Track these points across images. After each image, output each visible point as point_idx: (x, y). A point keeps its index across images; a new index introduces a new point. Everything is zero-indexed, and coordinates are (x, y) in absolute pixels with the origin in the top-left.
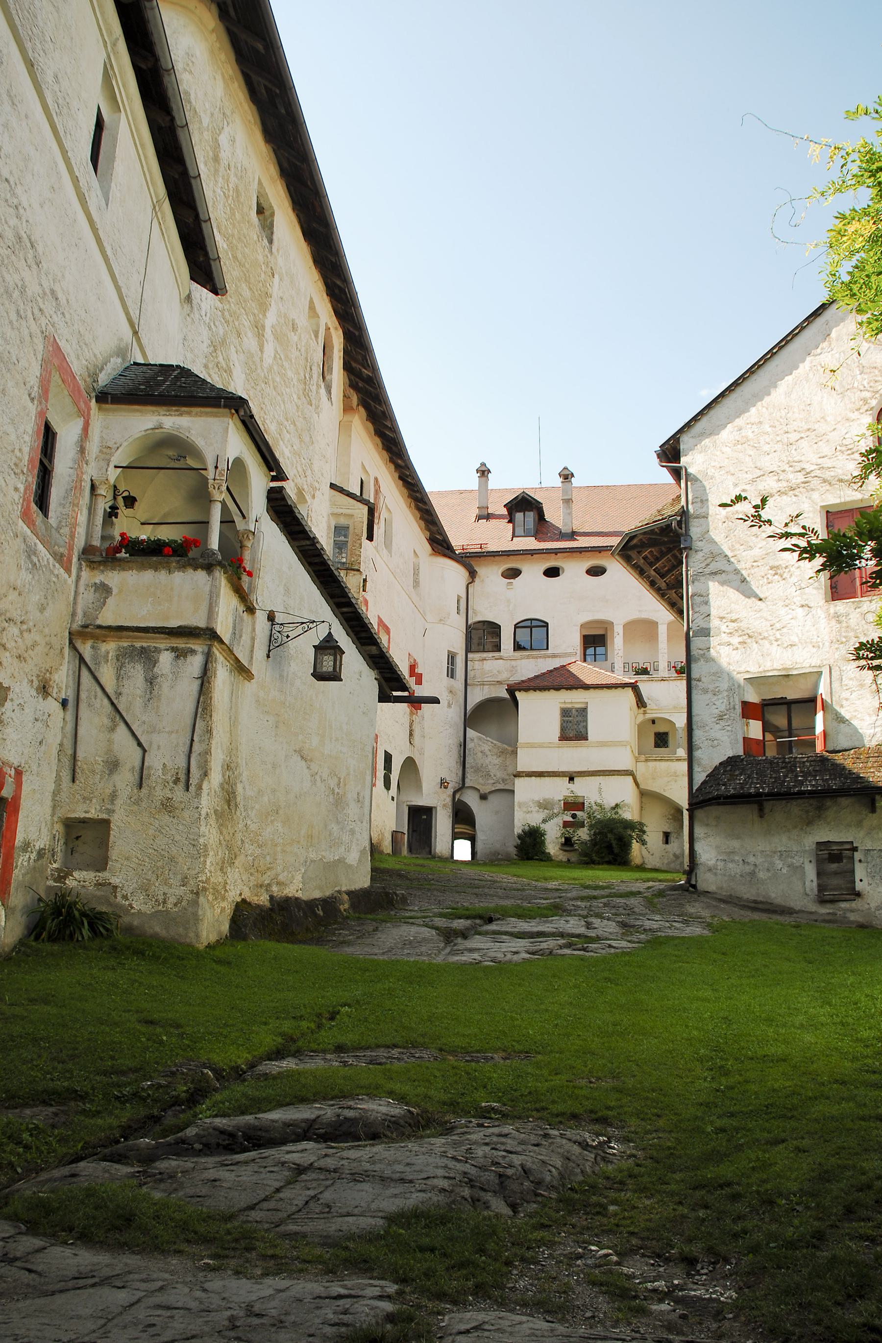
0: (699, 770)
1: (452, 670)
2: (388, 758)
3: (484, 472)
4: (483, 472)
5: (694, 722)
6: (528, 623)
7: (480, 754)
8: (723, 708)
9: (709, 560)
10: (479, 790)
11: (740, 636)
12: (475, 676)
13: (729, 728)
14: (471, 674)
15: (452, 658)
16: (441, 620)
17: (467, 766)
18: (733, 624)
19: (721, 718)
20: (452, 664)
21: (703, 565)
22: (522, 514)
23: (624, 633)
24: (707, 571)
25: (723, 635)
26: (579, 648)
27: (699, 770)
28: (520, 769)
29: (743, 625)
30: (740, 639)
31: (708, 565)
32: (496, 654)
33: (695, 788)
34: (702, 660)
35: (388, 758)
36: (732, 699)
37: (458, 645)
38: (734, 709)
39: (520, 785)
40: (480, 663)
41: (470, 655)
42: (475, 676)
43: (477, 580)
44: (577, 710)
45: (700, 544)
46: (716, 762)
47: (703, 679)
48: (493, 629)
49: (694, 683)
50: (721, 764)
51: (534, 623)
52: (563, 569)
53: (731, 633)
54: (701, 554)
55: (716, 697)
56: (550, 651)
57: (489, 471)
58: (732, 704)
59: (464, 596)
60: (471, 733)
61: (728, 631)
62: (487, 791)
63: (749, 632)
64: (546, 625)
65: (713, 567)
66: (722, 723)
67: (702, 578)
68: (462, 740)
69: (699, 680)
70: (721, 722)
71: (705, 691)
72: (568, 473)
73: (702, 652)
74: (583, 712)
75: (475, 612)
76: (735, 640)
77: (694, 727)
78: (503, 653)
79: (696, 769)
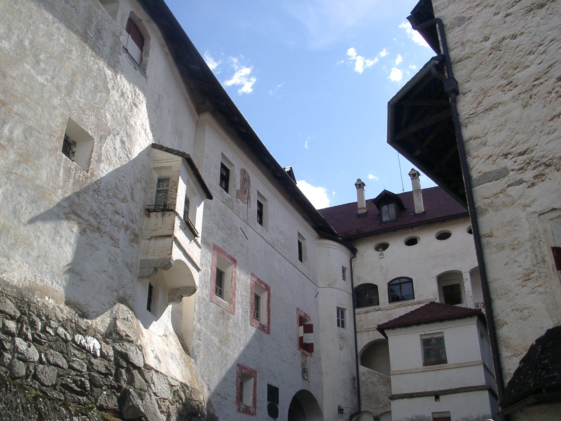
0: (509, 354)
1: (343, 322)
2: (273, 392)
3: (360, 185)
4: (360, 185)
5: (491, 290)
6: (398, 281)
7: (370, 385)
8: (528, 264)
9: (480, 99)
10: (372, 413)
11: (534, 168)
12: (362, 326)
13: (541, 289)
14: (358, 324)
15: (341, 312)
16: (329, 285)
17: (362, 394)
18: (521, 157)
19: (527, 278)
20: (343, 317)
21: (475, 105)
22: (386, 206)
23: (471, 279)
24: (480, 109)
25: (511, 173)
26: (437, 294)
27: (509, 354)
28: (394, 392)
29: (536, 154)
30: (536, 172)
31: (480, 103)
32: (376, 307)
33: (507, 380)
34: (490, 210)
35: (273, 392)
36: (538, 250)
37: (347, 302)
38: (544, 261)
39: (396, 405)
40: (365, 315)
41: (357, 310)
42: (362, 326)
43: (358, 255)
44: (436, 339)
45: (467, 85)
46: (531, 341)
47: (495, 233)
48: (372, 288)
49: (484, 240)
50: (538, 341)
51: (402, 280)
52: (419, 238)
53: (521, 169)
54: (470, 95)
55: (516, 252)
56: (416, 300)
57: (364, 185)
58: (539, 256)
59: (347, 266)
60: (362, 369)
61: (517, 167)
62: (379, 414)
63: (545, 160)
64: (410, 281)
65: (486, 103)
66: (531, 284)
67: (475, 118)
68: (355, 375)
69: (490, 236)
70: (528, 283)
71: (501, 247)
72: (415, 172)
73: (488, 201)
74: (440, 341)
75: (358, 279)
76: (528, 175)
77: (493, 296)
78: (381, 306)
79: (505, 353)
